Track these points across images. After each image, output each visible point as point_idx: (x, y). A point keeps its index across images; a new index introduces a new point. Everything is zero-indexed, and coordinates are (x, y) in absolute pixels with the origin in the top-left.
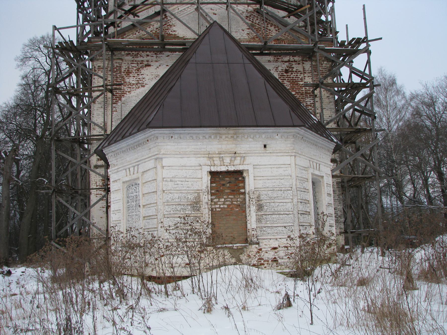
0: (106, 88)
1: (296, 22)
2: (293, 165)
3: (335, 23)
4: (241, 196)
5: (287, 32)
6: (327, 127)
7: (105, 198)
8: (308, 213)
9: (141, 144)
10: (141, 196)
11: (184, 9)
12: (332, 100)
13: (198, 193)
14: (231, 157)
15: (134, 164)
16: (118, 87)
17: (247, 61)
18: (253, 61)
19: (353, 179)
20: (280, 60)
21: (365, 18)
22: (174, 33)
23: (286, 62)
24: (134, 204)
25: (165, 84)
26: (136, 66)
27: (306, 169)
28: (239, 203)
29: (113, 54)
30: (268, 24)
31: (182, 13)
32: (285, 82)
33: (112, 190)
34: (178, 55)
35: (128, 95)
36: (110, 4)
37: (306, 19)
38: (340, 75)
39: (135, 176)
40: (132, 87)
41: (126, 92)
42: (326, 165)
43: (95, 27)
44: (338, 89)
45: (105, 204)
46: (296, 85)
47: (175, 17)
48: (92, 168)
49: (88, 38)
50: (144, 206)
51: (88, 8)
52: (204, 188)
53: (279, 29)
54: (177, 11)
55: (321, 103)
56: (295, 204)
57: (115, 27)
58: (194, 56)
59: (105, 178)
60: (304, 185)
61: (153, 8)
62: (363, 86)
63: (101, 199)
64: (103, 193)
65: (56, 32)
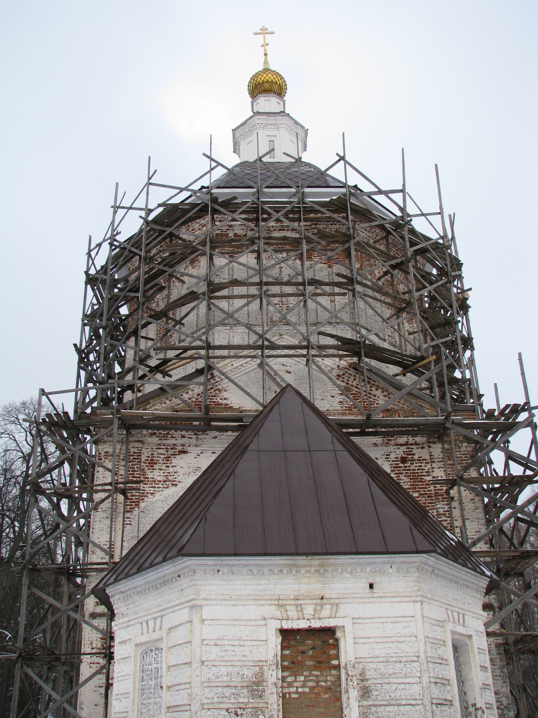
0: (116, 487)
1: (415, 383)
2: (419, 617)
3: (477, 381)
4: (333, 672)
5: (402, 398)
6: (473, 549)
7: (105, 671)
8: (448, 703)
9: (167, 581)
10: (164, 669)
11: (241, 365)
12: (480, 504)
13: (260, 665)
14: (316, 605)
15: (155, 615)
16: (134, 485)
17: (339, 447)
18: (349, 448)
19: (524, 639)
20: (392, 442)
21: (523, 374)
22: (224, 402)
23: (402, 445)
24: (152, 683)
25: (209, 484)
26: (165, 453)
27: (441, 624)
28: (329, 683)
29: (129, 433)
30: (371, 387)
31: (238, 371)
32: (402, 477)
33: (116, 656)
34: (229, 437)
35: (150, 499)
36: (128, 356)
37: (431, 378)
38: (491, 462)
39: (155, 636)
40: (157, 486)
41: (147, 493)
42: (475, 615)
43: (104, 390)
44: (488, 486)
45: (104, 681)
46: (419, 482)
47: (227, 377)
48: (87, 618)
49: (92, 408)
50: (169, 687)
51: (95, 362)
52: (270, 657)
53: (389, 394)
54: (229, 368)
55: (462, 510)
56: (425, 685)
57: (133, 392)
58: (255, 440)
59: (106, 635)
60: (440, 652)
61: (193, 364)
62: (529, 480)
63: (98, 672)
64: (102, 662)
65: (44, 398)
